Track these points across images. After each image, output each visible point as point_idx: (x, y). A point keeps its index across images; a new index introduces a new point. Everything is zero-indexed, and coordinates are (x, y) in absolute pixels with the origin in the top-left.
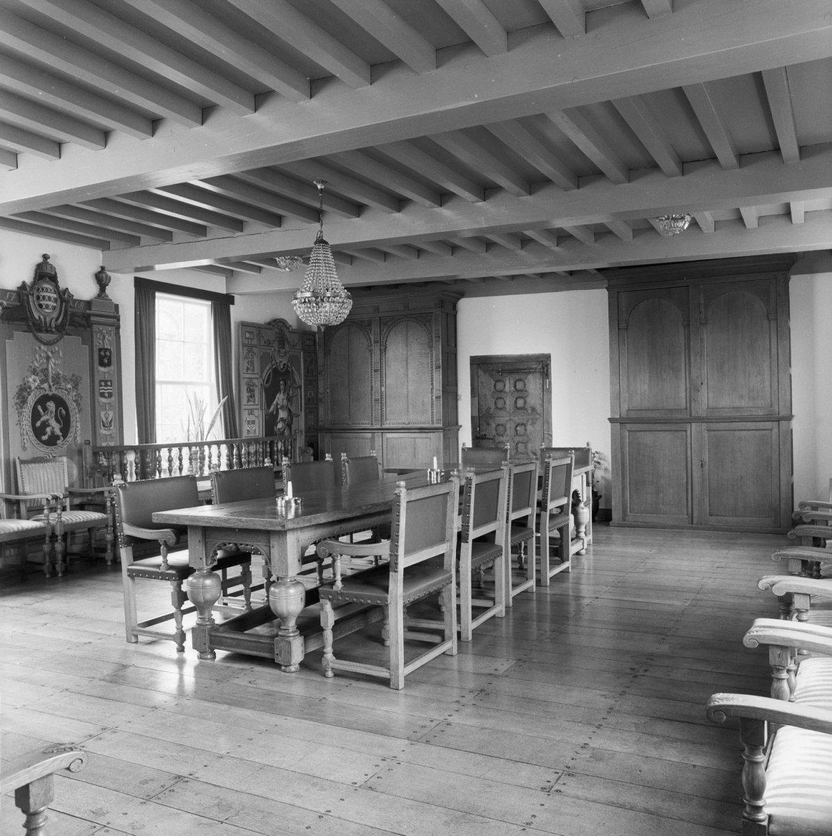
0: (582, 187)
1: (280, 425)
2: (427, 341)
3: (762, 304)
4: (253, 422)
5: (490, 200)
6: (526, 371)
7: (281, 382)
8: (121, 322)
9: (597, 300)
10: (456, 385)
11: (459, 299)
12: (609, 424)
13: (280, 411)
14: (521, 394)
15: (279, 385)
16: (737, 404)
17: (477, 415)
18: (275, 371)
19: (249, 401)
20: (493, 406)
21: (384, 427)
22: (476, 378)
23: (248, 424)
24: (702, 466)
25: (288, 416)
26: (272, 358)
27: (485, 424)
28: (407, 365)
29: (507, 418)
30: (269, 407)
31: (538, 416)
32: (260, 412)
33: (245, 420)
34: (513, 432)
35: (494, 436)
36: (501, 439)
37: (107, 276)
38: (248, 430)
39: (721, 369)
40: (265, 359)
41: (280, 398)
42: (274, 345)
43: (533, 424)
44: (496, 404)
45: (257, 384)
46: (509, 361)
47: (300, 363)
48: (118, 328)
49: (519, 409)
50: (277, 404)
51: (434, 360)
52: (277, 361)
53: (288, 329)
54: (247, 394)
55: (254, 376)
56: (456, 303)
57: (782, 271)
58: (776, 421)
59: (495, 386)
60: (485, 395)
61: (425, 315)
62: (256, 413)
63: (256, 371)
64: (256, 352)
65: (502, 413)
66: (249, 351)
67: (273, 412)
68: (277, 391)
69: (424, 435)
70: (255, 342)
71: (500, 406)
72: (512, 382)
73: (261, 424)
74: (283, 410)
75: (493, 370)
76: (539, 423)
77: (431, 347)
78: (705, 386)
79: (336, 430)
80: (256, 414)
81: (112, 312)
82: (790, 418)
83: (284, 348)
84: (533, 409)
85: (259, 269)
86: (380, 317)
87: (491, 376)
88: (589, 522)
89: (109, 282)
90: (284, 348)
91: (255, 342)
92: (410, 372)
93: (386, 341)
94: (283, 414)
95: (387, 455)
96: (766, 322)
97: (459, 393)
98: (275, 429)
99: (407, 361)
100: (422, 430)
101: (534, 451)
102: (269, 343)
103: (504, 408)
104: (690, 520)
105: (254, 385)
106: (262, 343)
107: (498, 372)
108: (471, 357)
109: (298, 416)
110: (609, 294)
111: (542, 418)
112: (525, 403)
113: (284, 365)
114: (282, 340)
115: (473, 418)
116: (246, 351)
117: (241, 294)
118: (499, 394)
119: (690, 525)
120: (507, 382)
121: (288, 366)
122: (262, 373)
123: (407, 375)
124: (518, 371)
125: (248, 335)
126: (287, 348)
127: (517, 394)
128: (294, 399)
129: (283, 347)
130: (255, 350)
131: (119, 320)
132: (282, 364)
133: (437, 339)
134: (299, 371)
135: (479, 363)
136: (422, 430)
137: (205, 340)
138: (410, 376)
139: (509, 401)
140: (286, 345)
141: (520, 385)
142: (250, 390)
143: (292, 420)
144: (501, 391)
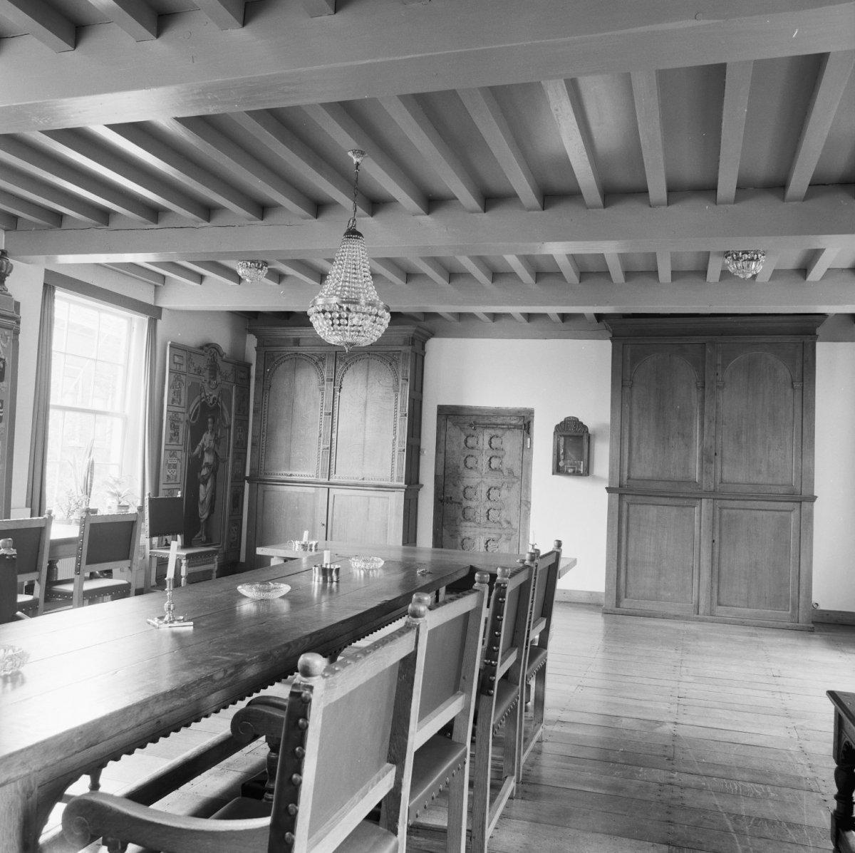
0: (673, 204)
1: (204, 472)
2: (391, 385)
3: (786, 370)
4: (175, 466)
5: (489, 212)
6: (502, 427)
7: (210, 420)
8: (22, 326)
9: (600, 352)
10: (420, 437)
11: (428, 338)
12: (606, 494)
14: (497, 453)
15: (207, 423)
16: (755, 479)
18: (204, 405)
19: (171, 439)
21: (332, 480)
22: (443, 432)
26: (201, 390)
27: (451, 484)
30: (193, 448)
31: (516, 480)
34: (484, 496)
35: (462, 500)
37: (8, 263)
38: (168, 476)
39: (738, 439)
40: (195, 390)
41: (207, 439)
43: (509, 488)
45: (182, 419)
46: (485, 414)
47: (231, 398)
48: (17, 333)
50: (203, 445)
51: (399, 405)
52: (207, 394)
53: (221, 356)
54: (171, 432)
55: (181, 410)
56: (426, 341)
57: (811, 335)
58: (799, 502)
59: (466, 442)
61: (391, 353)
62: (179, 454)
63: (182, 404)
64: (184, 380)
65: (473, 473)
66: (177, 379)
68: (205, 429)
70: (184, 368)
71: (469, 465)
75: (465, 423)
76: (517, 486)
77: (396, 391)
78: (718, 457)
79: (277, 481)
81: (9, 311)
82: (812, 499)
84: (511, 472)
85: (201, 278)
86: (336, 352)
87: (462, 429)
88: (141, 509)
89: (10, 272)
91: (184, 368)
94: (208, 459)
96: (790, 390)
97: (422, 447)
98: (199, 477)
99: (365, 405)
100: (379, 487)
102: (199, 371)
104: (696, 609)
106: (192, 371)
107: (471, 425)
110: (613, 346)
113: (214, 399)
114: (214, 369)
115: (436, 477)
119: (695, 616)
121: (218, 401)
122: (189, 406)
123: (365, 422)
124: (495, 426)
125: (177, 359)
126: (219, 379)
127: (491, 453)
129: (214, 378)
130: (183, 378)
131: (18, 323)
133: (405, 382)
136: (379, 487)
138: (368, 423)
140: (219, 377)
141: (495, 443)
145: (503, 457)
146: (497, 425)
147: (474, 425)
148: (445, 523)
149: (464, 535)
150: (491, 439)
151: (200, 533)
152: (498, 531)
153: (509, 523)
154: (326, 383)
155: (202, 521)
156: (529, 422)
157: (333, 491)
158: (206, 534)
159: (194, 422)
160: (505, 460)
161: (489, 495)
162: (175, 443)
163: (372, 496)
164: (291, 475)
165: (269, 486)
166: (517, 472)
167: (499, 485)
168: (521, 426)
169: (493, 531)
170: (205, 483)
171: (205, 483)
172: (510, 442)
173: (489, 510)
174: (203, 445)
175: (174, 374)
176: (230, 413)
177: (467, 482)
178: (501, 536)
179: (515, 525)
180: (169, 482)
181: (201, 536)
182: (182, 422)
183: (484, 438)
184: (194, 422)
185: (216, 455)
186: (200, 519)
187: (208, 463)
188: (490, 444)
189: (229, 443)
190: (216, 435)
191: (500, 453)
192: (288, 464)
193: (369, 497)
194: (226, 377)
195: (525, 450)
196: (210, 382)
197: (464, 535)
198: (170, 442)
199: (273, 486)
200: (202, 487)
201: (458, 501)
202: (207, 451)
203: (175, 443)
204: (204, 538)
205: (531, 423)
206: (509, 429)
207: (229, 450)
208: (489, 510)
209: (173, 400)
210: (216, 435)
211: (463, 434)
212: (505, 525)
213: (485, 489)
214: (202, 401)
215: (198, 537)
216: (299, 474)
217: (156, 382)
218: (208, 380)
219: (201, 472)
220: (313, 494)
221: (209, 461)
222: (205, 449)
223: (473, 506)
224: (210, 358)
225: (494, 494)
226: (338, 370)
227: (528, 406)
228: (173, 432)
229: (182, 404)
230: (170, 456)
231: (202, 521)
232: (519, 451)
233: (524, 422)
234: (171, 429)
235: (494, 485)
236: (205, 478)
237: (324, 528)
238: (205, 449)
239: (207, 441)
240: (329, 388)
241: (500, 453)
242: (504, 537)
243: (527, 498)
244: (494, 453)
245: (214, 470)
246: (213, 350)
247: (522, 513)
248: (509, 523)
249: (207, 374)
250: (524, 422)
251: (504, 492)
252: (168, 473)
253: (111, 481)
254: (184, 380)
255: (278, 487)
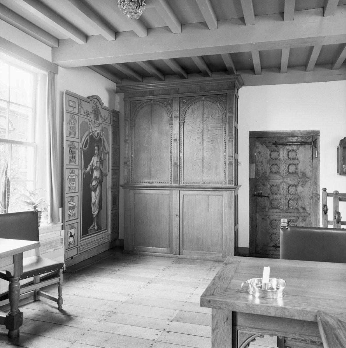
1: (94, 183)
4: (74, 180)
7: (96, 148)
13: (95, 171)
14: (293, 161)
15: (94, 150)
17: (254, 177)
18: (91, 137)
19: (70, 161)
20: (268, 171)
23: (70, 181)
24: (208, 204)
25: (100, 175)
28: (203, 136)
29: (281, 180)
30: (86, 167)
32: (80, 171)
33: (67, 178)
35: (269, 194)
36: (275, 196)
38: (69, 187)
41: (95, 160)
42: (91, 116)
44: (271, 169)
45: (77, 147)
49: (290, 173)
50: (93, 165)
52: (93, 130)
54: (70, 156)
60: (262, 162)
62: (76, 171)
63: (77, 136)
64: (77, 119)
65: (277, 176)
66: (72, 118)
67: (89, 172)
68: (93, 154)
69: (217, 193)
70: (76, 110)
72: (285, 152)
73: (80, 182)
74: (97, 170)
75: (269, 143)
76: (308, 184)
79: (140, 187)
80: (77, 174)
83: (98, 120)
84: (304, 174)
87: (267, 147)
90: (98, 120)
91: (76, 110)
92: (205, 142)
93: (185, 117)
94: (96, 174)
95: (183, 208)
98: (91, 186)
99: (203, 133)
100: (216, 189)
101: (303, 206)
103: (279, 172)
105: (75, 148)
106: (83, 113)
108: (249, 132)
109: (107, 175)
111: (310, 181)
112: (296, 169)
113: (98, 134)
115: (250, 180)
116: (69, 118)
117: (63, 67)
118: (274, 162)
120: (281, 153)
121: (100, 135)
122: (81, 138)
123: (203, 144)
125: (71, 103)
126: (100, 120)
128: (104, 162)
129: (97, 119)
132: (96, 133)
134: (107, 140)
135: (257, 138)
136: (216, 189)
137: (1, 292)
138: (205, 145)
139: (283, 168)
142: (72, 152)
143: (102, 179)
144: (276, 159)
145: (298, 164)
146: (293, 142)
147: (276, 144)
148: (258, 210)
149: (271, 218)
150: (288, 153)
151: (93, 224)
152: (296, 215)
153: (304, 209)
154: (174, 119)
155: (94, 216)
156: (316, 140)
157: (183, 192)
158: (98, 225)
159: (86, 149)
160: (300, 166)
161: (289, 190)
162: (73, 163)
163: (210, 195)
164: (153, 183)
165: (137, 190)
166: (309, 174)
167: (296, 184)
168: (310, 142)
169: (292, 214)
170: (95, 190)
171: (95, 190)
172: (303, 154)
173: (289, 201)
174: (93, 165)
175: (70, 114)
176: (108, 142)
177: (272, 182)
178: (298, 217)
179: (308, 210)
180: (70, 192)
181: (94, 226)
182: (77, 149)
183: (283, 153)
184: (86, 149)
185: (101, 172)
186: (93, 215)
187: (96, 177)
188: (288, 155)
189: (109, 163)
190: (100, 158)
191: (296, 162)
192: (150, 176)
193: (208, 195)
194: (105, 120)
195: (314, 158)
196: (95, 122)
197: (271, 218)
198: (70, 163)
199: (140, 190)
200: (93, 193)
201: (267, 195)
202: (95, 169)
203: (73, 163)
204: (96, 228)
205: (318, 140)
206: (301, 145)
207: (109, 168)
208: (289, 201)
209: (70, 133)
210: (100, 158)
211: (268, 150)
212: (301, 210)
213: (285, 187)
214: (91, 134)
215: (92, 227)
216: (156, 181)
217: (100, 233)
218: (93, 120)
219: (92, 183)
220: (169, 195)
221: (97, 176)
222: (94, 168)
223: (278, 198)
224: (94, 105)
225: (292, 189)
226: (182, 110)
227: (315, 128)
228: (71, 156)
229: (77, 136)
230: (71, 174)
231: (94, 216)
232: (310, 160)
233: (311, 140)
234: (70, 154)
235: (292, 183)
236: (95, 187)
237: (178, 217)
238: (94, 168)
239: (95, 162)
240: (176, 122)
241: (296, 162)
242: (301, 218)
243: (317, 191)
244: (292, 162)
245: (100, 182)
246: (95, 100)
247: (314, 202)
248: (304, 209)
249: (92, 116)
250: (311, 140)
251: (300, 189)
252: (70, 186)
253: (28, 194)
254: (77, 119)
255: (143, 191)
